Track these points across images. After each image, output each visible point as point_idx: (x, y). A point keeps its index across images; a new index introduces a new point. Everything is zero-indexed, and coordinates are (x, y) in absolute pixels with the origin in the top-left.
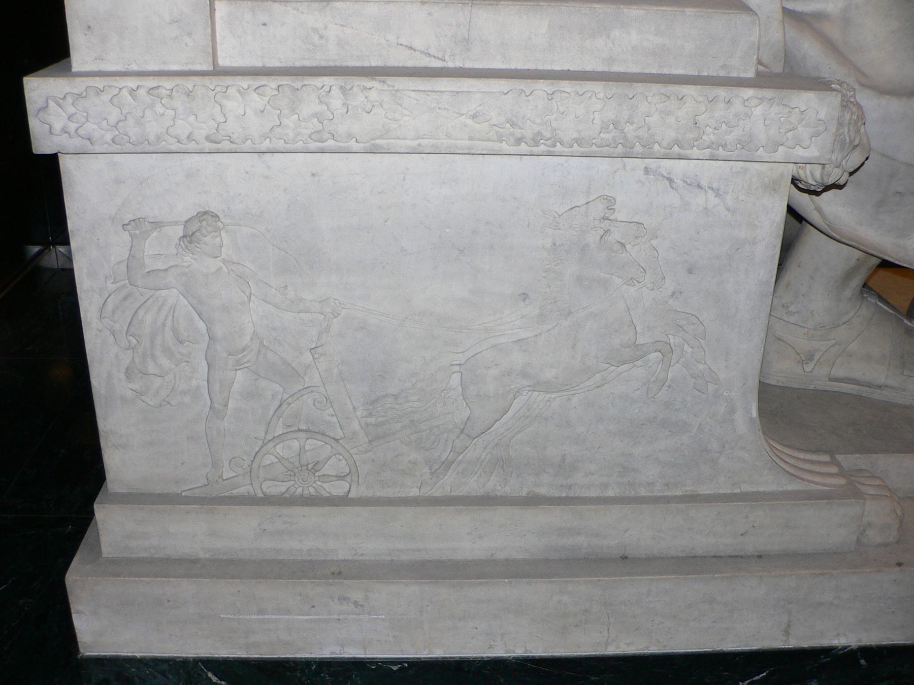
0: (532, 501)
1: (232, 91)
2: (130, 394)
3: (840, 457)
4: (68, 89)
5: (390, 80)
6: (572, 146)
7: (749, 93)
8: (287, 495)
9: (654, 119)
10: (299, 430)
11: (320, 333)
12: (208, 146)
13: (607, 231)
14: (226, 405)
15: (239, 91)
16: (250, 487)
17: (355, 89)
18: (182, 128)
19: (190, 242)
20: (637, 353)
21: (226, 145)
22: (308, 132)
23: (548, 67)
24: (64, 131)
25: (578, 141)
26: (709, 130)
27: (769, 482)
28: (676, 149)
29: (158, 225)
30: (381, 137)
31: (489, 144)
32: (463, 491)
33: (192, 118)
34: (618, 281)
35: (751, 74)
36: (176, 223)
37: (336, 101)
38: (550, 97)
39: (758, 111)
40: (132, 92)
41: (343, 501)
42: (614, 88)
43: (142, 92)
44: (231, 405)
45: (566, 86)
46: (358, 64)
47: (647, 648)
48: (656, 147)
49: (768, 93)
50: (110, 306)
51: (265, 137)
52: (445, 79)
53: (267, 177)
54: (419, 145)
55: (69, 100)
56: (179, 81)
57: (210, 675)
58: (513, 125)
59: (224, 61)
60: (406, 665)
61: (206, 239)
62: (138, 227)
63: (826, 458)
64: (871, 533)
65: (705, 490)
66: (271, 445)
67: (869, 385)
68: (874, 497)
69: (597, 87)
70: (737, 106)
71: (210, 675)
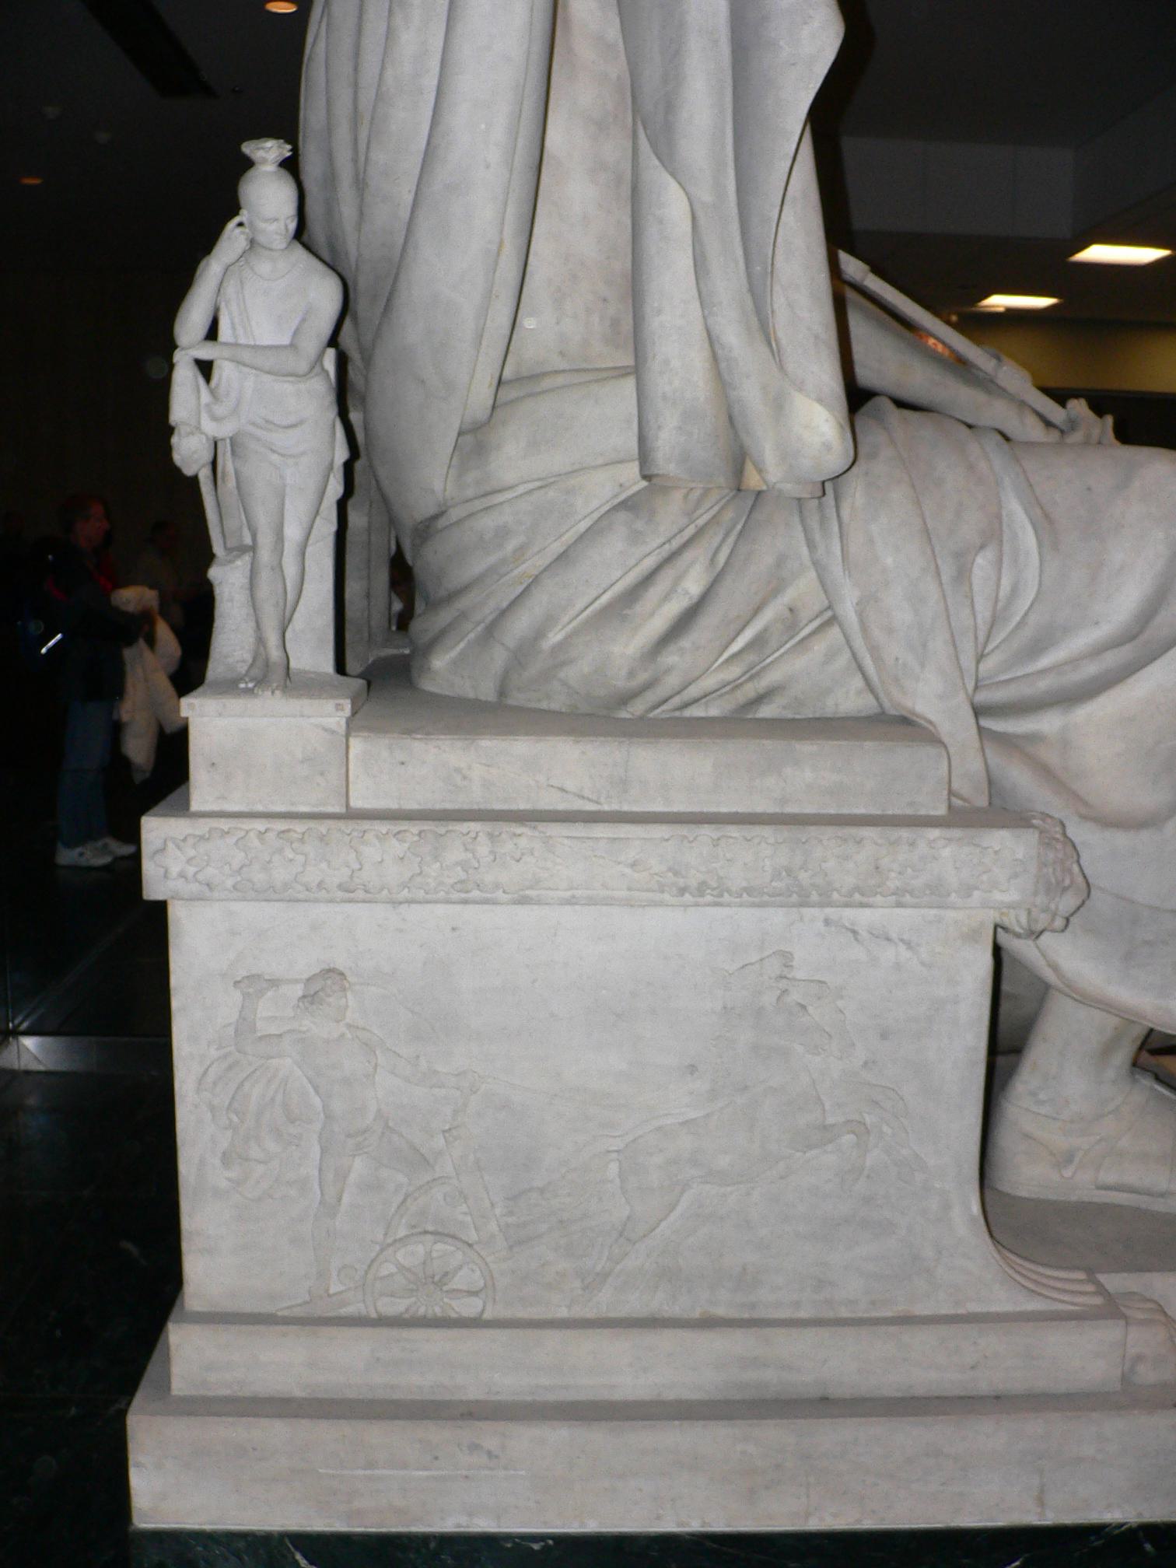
0: (708, 1323)
1: (369, 836)
2: (224, 1184)
3: (1102, 1278)
4: (190, 831)
5: (541, 826)
6: (741, 896)
7: (934, 833)
8: (407, 1316)
9: (831, 864)
10: (426, 1232)
11: (456, 1112)
12: (340, 894)
13: (785, 992)
14: (340, 1200)
15: (377, 837)
16: (361, 1306)
17: (504, 836)
18: (312, 876)
19: (312, 1003)
20: (826, 1133)
21: (360, 894)
22: (452, 881)
23: (713, 809)
24: (182, 875)
25: (748, 890)
26: (893, 875)
27: (1003, 1299)
28: (857, 897)
29: (274, 983)
30: (531, 888)
31: (650, 895)
32: (622, 1312)
33: (324, 865)
34: (800, 1049)
35: (941, 810)
36: (296, 981)
37: (483, 849)
38: (716, 843)
39: (946, 852)
40: (261, 835)
41: (475, 1323)
42: (785, 832)
43: (271, 835)
44: (346, 1199)
45: (733, 831)
46: (505, 807)
47: (859, 1521)
48: (835, 896)
49: (957, 833)
50: (210, 1078)
51: (404, 886)
52: (602, 825)
53: (401, 931)
54: (573, 897)
55: (191, 841)
56: (312, 824)
57: (298, 1557)
58: (676, 874)
59: (357, 803)
60: (551, 1542)
61: (331, 1000)
62: (254, 985)
63: (1081, 1275)
64: (1141, 1368)
65: (922, 1309)
66: (390, 1250)
67: (1149, 1193)
68: (1143, 1323)
69: (767, 831)
70: (922, 847)
71: (298, 1557)
